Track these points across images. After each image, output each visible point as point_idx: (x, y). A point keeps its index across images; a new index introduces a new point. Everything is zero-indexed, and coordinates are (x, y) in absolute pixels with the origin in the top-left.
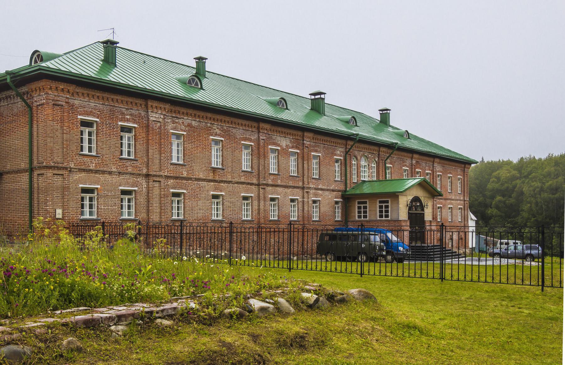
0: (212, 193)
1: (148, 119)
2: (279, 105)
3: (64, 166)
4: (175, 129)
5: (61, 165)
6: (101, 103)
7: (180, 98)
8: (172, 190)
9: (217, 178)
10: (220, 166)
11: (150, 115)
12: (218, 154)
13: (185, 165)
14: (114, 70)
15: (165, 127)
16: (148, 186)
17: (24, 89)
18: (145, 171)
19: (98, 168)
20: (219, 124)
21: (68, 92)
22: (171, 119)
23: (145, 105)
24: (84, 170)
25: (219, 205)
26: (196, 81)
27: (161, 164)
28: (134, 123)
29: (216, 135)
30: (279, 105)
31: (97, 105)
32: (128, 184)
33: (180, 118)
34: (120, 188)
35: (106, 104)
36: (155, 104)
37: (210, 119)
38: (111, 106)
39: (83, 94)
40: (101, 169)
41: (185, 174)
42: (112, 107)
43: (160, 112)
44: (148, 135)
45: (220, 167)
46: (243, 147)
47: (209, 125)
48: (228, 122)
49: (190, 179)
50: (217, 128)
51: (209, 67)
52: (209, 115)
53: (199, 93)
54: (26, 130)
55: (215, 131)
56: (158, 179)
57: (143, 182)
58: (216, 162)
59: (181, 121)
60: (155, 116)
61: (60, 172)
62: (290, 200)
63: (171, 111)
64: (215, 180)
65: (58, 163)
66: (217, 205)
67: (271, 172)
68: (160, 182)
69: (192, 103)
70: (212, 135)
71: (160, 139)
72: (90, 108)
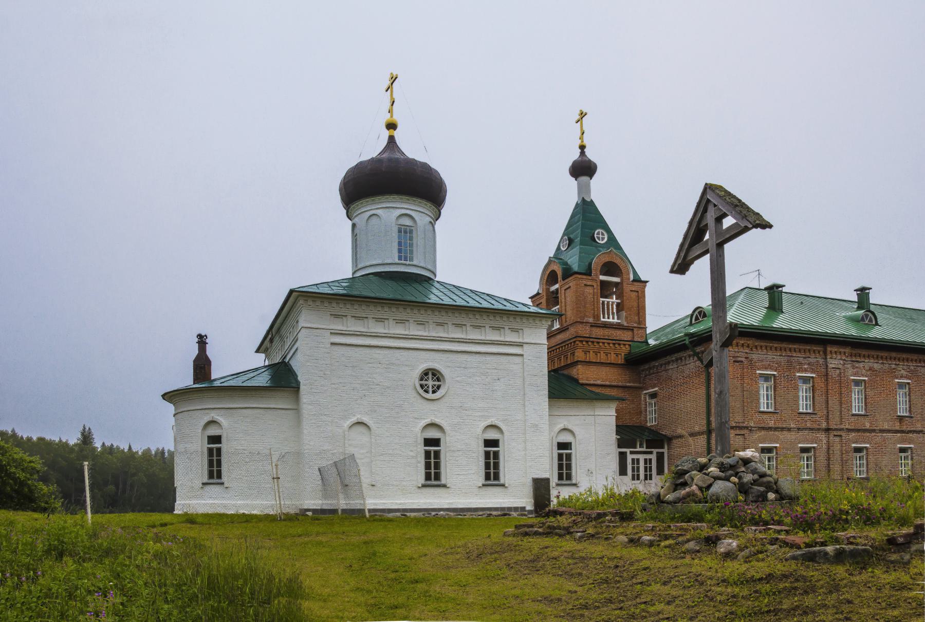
0: (899, 446)
1: (827, 366)
2: (864, 321)
3: (745, 425)
4: (855, 375)
5: (741, 425)
6: (779, 354)
7: (864, 338)
8: (853, 445)
9: (904, 428)
10: (810, 409)
11: (829, 362)
12: (769, 393)
13: (867, 415)
14: (781, 315)
15: (844, 373)
16: (828, 442)
17: (698, 349)
18: (824, 425)
19: (777, 425)
20: (905, 364)
21: (748, 346)
22: (851, 364)
23: (823, 352)
24: (763, 428)
25: (809, 460)
26: (870, 317)
27: (841, 416)
28: (812, 373)
29: (902, 377)
30: (864, 321)
31: (775, 357)
32: (807, 440)
33: (861, 362)
34: (800, 445)
35: (783, 354)
36: (834, 349)
37: (895, 359)
38: (788, 356)
39: (761, 347)
40: (780, 426)
41: (868, 426)
42: (789, 358)
43: (839, 357)
44: (827, 384)
45: (907, 414)
46: (853, 384)
47: (893, 366)
48: (916, 361)
49: (874, 431)
50: (903, 369)
51: (874, 298)
52: (894, 355)
53: (759, 319)
54: (702, 391)
55: (900, 373)
56: (839, 433)
57: (822, 436)
58: (902, 410)
59: (861, 365)
60: (834, 362)
61: (742, 432)
62: (898, 451)
63: (851, 356)
64: (902, 431)
65: (739, 423)
66: (807, 461)
67: (899, 414)
68: (841, 436)
69: (798, 335)
70: (897, 378)
71: (840, 387)
72: (767, 361)
